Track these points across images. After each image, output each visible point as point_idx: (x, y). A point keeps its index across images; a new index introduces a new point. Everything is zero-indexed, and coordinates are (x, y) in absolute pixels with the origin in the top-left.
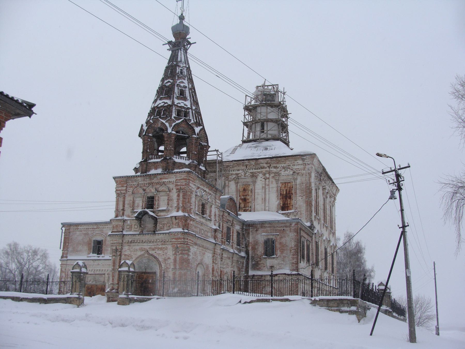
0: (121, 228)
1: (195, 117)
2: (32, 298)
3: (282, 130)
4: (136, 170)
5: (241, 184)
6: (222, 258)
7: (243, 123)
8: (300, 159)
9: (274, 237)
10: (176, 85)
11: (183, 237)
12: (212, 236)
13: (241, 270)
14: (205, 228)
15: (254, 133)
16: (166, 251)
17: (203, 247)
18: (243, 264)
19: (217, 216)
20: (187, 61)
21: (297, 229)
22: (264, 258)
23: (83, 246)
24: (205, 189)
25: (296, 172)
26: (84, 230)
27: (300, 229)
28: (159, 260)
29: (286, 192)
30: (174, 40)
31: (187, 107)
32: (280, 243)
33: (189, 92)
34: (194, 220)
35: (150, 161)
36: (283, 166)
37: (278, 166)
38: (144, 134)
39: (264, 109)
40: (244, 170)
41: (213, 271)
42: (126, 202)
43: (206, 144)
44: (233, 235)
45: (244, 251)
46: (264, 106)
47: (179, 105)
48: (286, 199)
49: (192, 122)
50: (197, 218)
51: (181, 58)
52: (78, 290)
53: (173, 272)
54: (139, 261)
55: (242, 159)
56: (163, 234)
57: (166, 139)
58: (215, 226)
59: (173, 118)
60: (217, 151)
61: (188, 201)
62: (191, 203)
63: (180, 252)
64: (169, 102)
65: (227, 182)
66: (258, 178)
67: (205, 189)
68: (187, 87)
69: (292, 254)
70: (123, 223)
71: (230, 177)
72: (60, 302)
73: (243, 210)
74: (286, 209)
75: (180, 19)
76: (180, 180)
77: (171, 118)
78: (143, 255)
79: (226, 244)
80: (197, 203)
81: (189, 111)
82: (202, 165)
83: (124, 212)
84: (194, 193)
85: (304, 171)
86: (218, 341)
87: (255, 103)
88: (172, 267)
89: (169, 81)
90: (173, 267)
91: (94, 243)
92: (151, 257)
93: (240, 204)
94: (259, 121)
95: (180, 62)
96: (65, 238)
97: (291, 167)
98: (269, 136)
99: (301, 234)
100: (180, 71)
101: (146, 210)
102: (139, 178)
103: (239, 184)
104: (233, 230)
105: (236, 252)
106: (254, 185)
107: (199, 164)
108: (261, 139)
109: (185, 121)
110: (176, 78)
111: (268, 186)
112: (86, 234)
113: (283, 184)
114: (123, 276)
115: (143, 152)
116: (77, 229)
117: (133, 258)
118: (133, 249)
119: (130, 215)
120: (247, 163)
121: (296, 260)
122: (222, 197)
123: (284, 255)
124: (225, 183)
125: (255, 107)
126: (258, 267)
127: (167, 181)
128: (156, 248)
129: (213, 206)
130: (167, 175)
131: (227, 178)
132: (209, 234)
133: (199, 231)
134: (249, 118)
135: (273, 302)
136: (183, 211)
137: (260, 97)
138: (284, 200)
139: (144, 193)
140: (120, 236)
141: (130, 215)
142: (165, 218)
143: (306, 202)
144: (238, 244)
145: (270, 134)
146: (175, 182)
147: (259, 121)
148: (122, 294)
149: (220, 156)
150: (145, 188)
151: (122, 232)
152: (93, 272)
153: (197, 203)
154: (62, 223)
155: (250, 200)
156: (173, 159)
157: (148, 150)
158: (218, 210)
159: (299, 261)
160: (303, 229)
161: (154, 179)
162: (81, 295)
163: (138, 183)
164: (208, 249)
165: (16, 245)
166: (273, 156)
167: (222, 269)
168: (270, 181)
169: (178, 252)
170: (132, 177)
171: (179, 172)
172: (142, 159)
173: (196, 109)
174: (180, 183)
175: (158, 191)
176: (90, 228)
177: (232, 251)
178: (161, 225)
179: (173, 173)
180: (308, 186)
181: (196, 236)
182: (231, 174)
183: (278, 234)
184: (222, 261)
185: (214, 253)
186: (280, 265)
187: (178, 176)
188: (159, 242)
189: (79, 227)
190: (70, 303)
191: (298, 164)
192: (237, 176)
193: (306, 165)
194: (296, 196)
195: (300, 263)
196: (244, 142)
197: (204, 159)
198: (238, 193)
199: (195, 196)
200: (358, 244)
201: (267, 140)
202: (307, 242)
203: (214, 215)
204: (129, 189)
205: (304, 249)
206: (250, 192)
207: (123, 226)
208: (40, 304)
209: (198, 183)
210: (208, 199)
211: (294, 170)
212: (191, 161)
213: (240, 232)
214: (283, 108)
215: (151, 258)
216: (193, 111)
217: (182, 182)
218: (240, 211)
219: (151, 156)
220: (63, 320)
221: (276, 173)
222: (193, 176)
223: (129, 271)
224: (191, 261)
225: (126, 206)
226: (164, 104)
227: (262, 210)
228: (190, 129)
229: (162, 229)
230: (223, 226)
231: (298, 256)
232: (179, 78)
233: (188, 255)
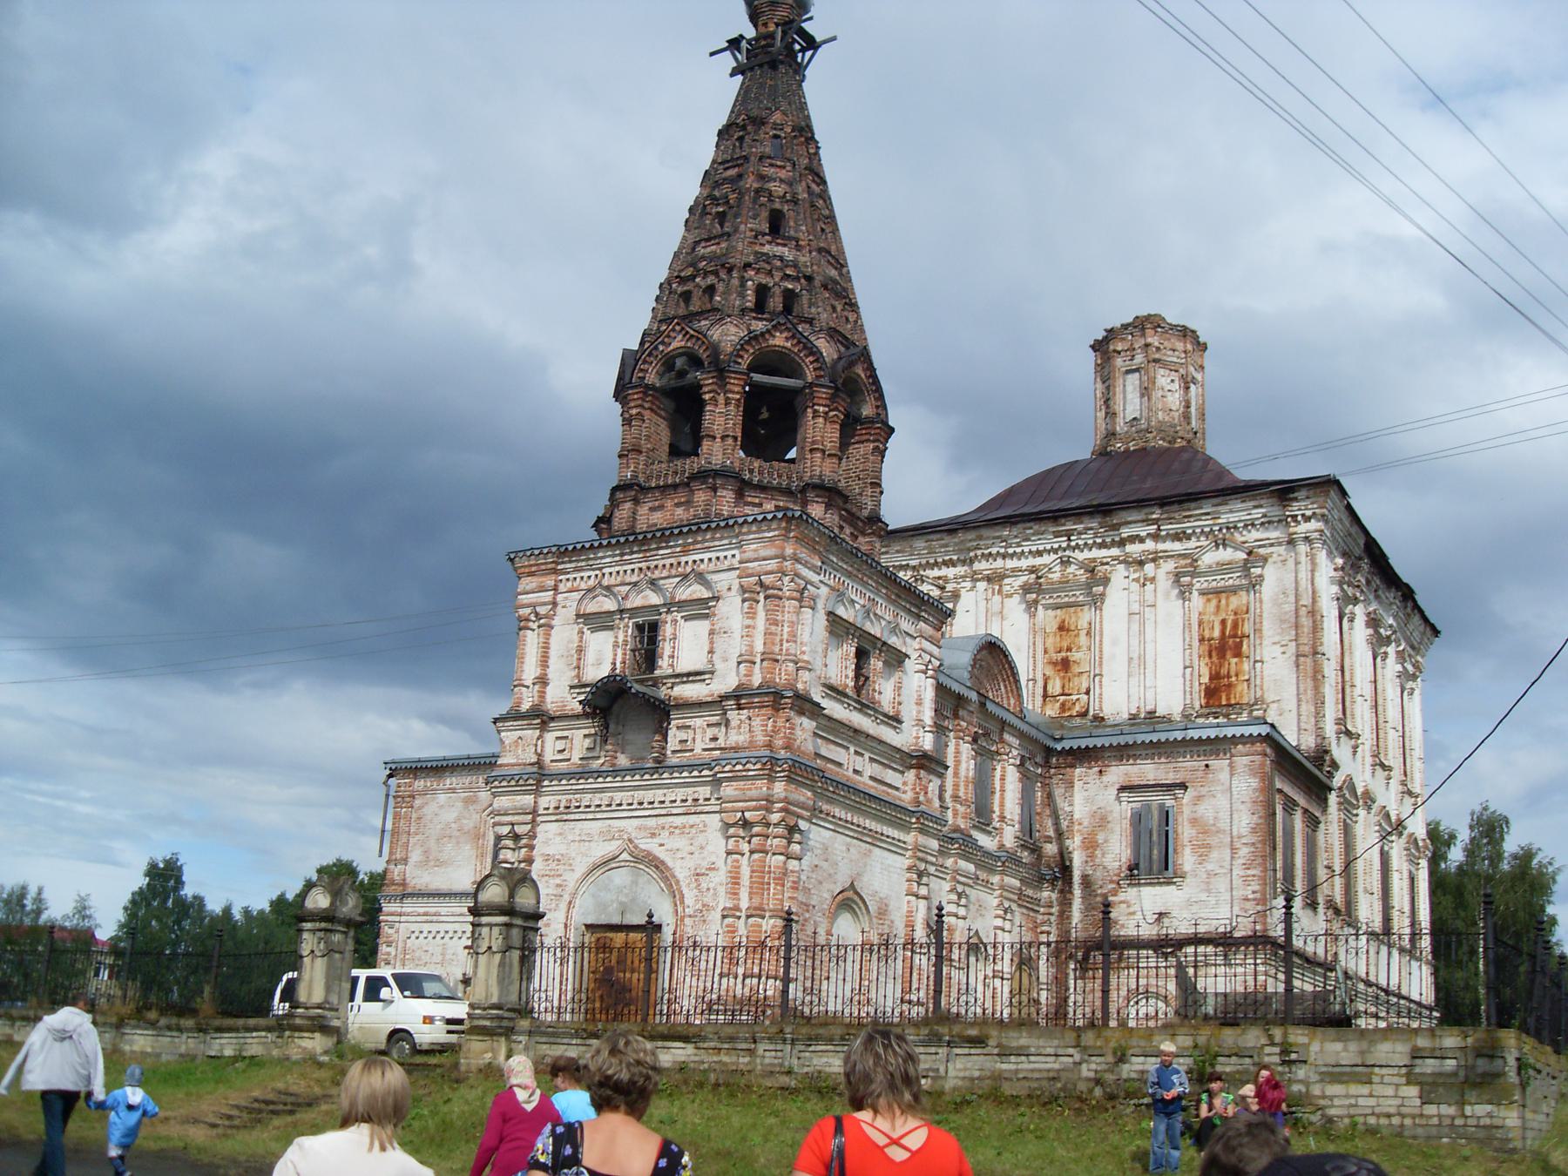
16: (701, 839)
23: (458, 843)
29: (1223, 632)
30: (750, 32)
32: (1194, 821)
42: (553, 653)
44: (1003, 791)
48: (1222, 655)
111: (1153, 609)
121: (1257, 888)
123: (1210, 867)
128: (663, 828)
138: (1215, 659)
192: (1033, 576)
200: (1526, 856)
206: (1083, 639)
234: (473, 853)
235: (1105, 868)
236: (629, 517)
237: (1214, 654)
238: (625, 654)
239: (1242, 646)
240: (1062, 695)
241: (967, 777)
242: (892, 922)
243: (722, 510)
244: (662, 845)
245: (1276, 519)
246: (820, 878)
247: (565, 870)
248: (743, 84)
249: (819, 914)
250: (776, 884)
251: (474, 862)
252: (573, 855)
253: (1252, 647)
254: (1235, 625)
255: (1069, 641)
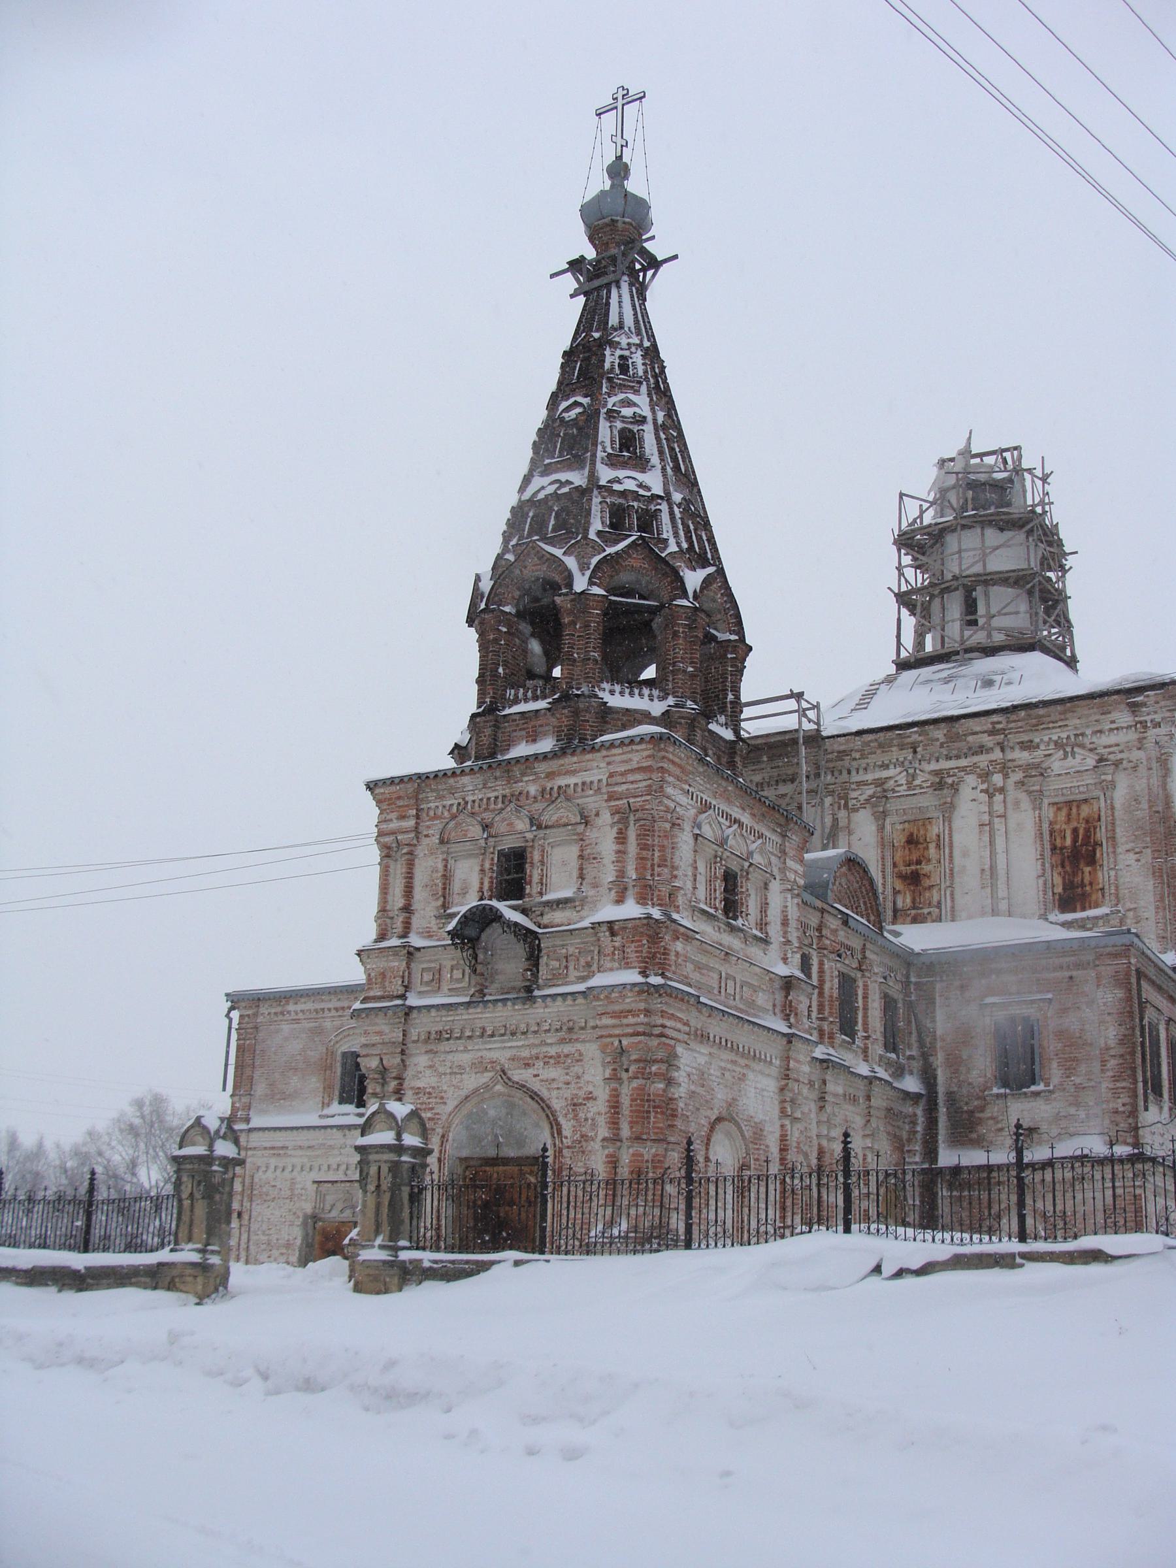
0: (400, 982)
1: (682, 533)
2: (30, 1266)
3: (1048, 612)
4: (458, 751)
5: (895, 819)
6: (822, 1099)
7: (896, 595)
8: (1123, 706)
9: (1031, 1011)
10: (602, 416)
11: (642, 1006)
12: (774, 1005)
13: (906, 1148)
14: (740, 972)
15: (939, 628)
16: (577, 1069)
17: (734, 1049)
18: (914, 1123)
19: (793, 924)
20: (643, 325)
21: (1128, 974)
22: (998, 1096)
24: (736, 813)
25: (1107, 760)
26: (308, 1015)
27: (1140, 974)
28: (549, 1107)
29: (1075, 840)
30: (591, 253)
31: (649, 494)
33: (658, 438)
34: (688, 936)
35: (507, 711)
36: (1055, 738)
37: (1037, 740)
38: (483, 606)
39: (970, 539)
40: (907, 763)
41: (783, 1150)
43: (734, 637)
44: (865, 1009)
45: (915, 1071)
46: (970, 527)
47: (616, 487)
48: (1076, 869)
49: (673, 547)
50: (707, 931)
51: (621, 315)
52: (200, 1231)
53: (606, 1152)
54: (470, 1115)
55: (897, 722)
56: (564, 1000)
57: (566, 620)
58: (785, 963)
59: (592, 535)
60: (799, 696)
61: (663, 859)
62: (674, 868)
63: (633, 1068)
64: (578, 478)
65: (842, 814)
66: (961, 790)
67: (734, 815)
68: (645, 417)
69: (1110, 1074)
70: (404, 963)
71: (854, 794)
72: (132, 1284)
73: (910, 918)
74: (1078, 907)
75: (611, 177)
76: (623, 774)
77: (585, 537)
78: (486, 1087)
79: (837, 1041)
80: (702, 868)
81: (658, 507)
82: (722, 719)
83: (409, 918)
84: (687, 827)
85: (1140, 754)
86: (728, 1473)
87: (934, 518)
88: (603, 1132)
89: (574, 407)
90: (607, 1135)
91: (344, 1065)
92: (519, 1094)
93: (896, 892)
94: (955, 583)
95: (615, 330)
96: (239, 1048)
97: (1087, 741)
98: (999, 638)
99: (1144, 996)
100: (617, 361)
101: (494, 903)
102: (466, 780)
103: (888, 821)
104: (866, 986)
105: (882, 1073)
106: (948, 820)
107: (709, 716)
108: (967, 651)
109: (642, 545)
110: (604, 390)
112: (318, 1031)
113: (1059, 809)
114: (373, 1170)
115: (481, 681)
116: (282, 1013)
117: (448, 1102)
118: (448, 1064)
119: (435, 928)
120: (914, 735)
121: (1127, 1100)
122: (807, 856)
123: (1078, 1081)
124: (835, 820)
125: (938, 534)
126: (974, 1136)
127: (576, 785)
128: (537, 1058)
129: (775, 886)
130: (575, 759)
131: (840, 798)
132: (762, 999)
133: (716, 986)
134: (915, 578)
135: (1030, 1267)
136: (642, 900)
137: (953, 497)
138: (1068, 868)
139: (485, 836)
140: (395, 1013)
141: (435, 928)
142: (571, 931)
143: (1154, 873)
144: (891, 1045)
145: (1000, 630)
146: (608, 785)
147: (955, 583)
148: (373, 1246)
149: (811, 714)
150: (488, 816)
151: (403, 997)
152: (341, 1172)
153: (702, 868)
154: (227, 995)
155: (935, 879)
156: (596, 696)
157: (501, 670)
158: (796, 901)
159: (1141, 1103)
160: (1151, 972)
161: (526, 779)
162: (213, 1252)
163: (464, 799)
164: (760, 1058)
165: (158, 1102)
166: (1015, 703)
167: (824, 1143)
168: (1009, 799)
169: (627, 1070)
170: (436, 776)
171: (622, 743)
172: (479, 707)
173: (686, 502)
174: (624, 787)
175: (539, 827)
176: (329, 1010)
177: (863, 1069)
178: (555, 964)
179: (597, 747)
180: (1160, 809)
181: (699, 1002)
182: (859, 783)
183: (1050, 996)
184: (822, 1108)
185: (786, 1075)
186: (1063, 1123)
187: (618, 758)
188: (548, 1031)
189: (291, 1007)
190: (171, 1286)
191: (1113, 726)
192: (879, 789)
193: (1145, 727)
194: (1114, 852)
195: (1146, 1109)
196: (903, 665)
197: (730, 697)
198: (888, 854)
199: (691, 841)
201: (990, 651)
202: (1167, 1029)
203: (779, 923)
204: (429, 827)
205: (1159, 1056)
206: (932, 851)
207: (406, 974)
208: (60, 1291)
209: (703, 787)
210: (750, 854)
211: (1101, 751)
212: (671, 701)
213: (896, 996)
214: (1043, 529)
215: (516, 1100)
216: (676, 510)
217: (632, 782)
218: (900, 920)
219: (513, 691)
220: (80, 1361)
221: (1027, 768)
222: (680, 758)
223: (399, 1149)
224: (681, 1105)
225: (419, 894)
226: (558, 488)
227: (983, 914)
228: (665, 575)
229: (558, 977)
230: (821, 971)
231: (1135, 1082)
232: (614, 388)
233: (670, 1082)
234: (320, 1086)
235: (970, 1084)
236: (490, 744)
237: (1067, 863)
238: (492, 882)
239: (1095, 854)
240: (914, 908)
241: (831, 997)
242: (767, 1146)
243: (586, 734)
244: (536, 1076)
245: (1125, 725)
246: (697, 1105)
247: (437, 1103)
248: (585, 305)
249: (698, 1142)
250: (656, 1113)
251: (321, 1095)
252: (445, 1088)
253: (1105, 855)
254: (1087, 836)
255: (918, 854)
